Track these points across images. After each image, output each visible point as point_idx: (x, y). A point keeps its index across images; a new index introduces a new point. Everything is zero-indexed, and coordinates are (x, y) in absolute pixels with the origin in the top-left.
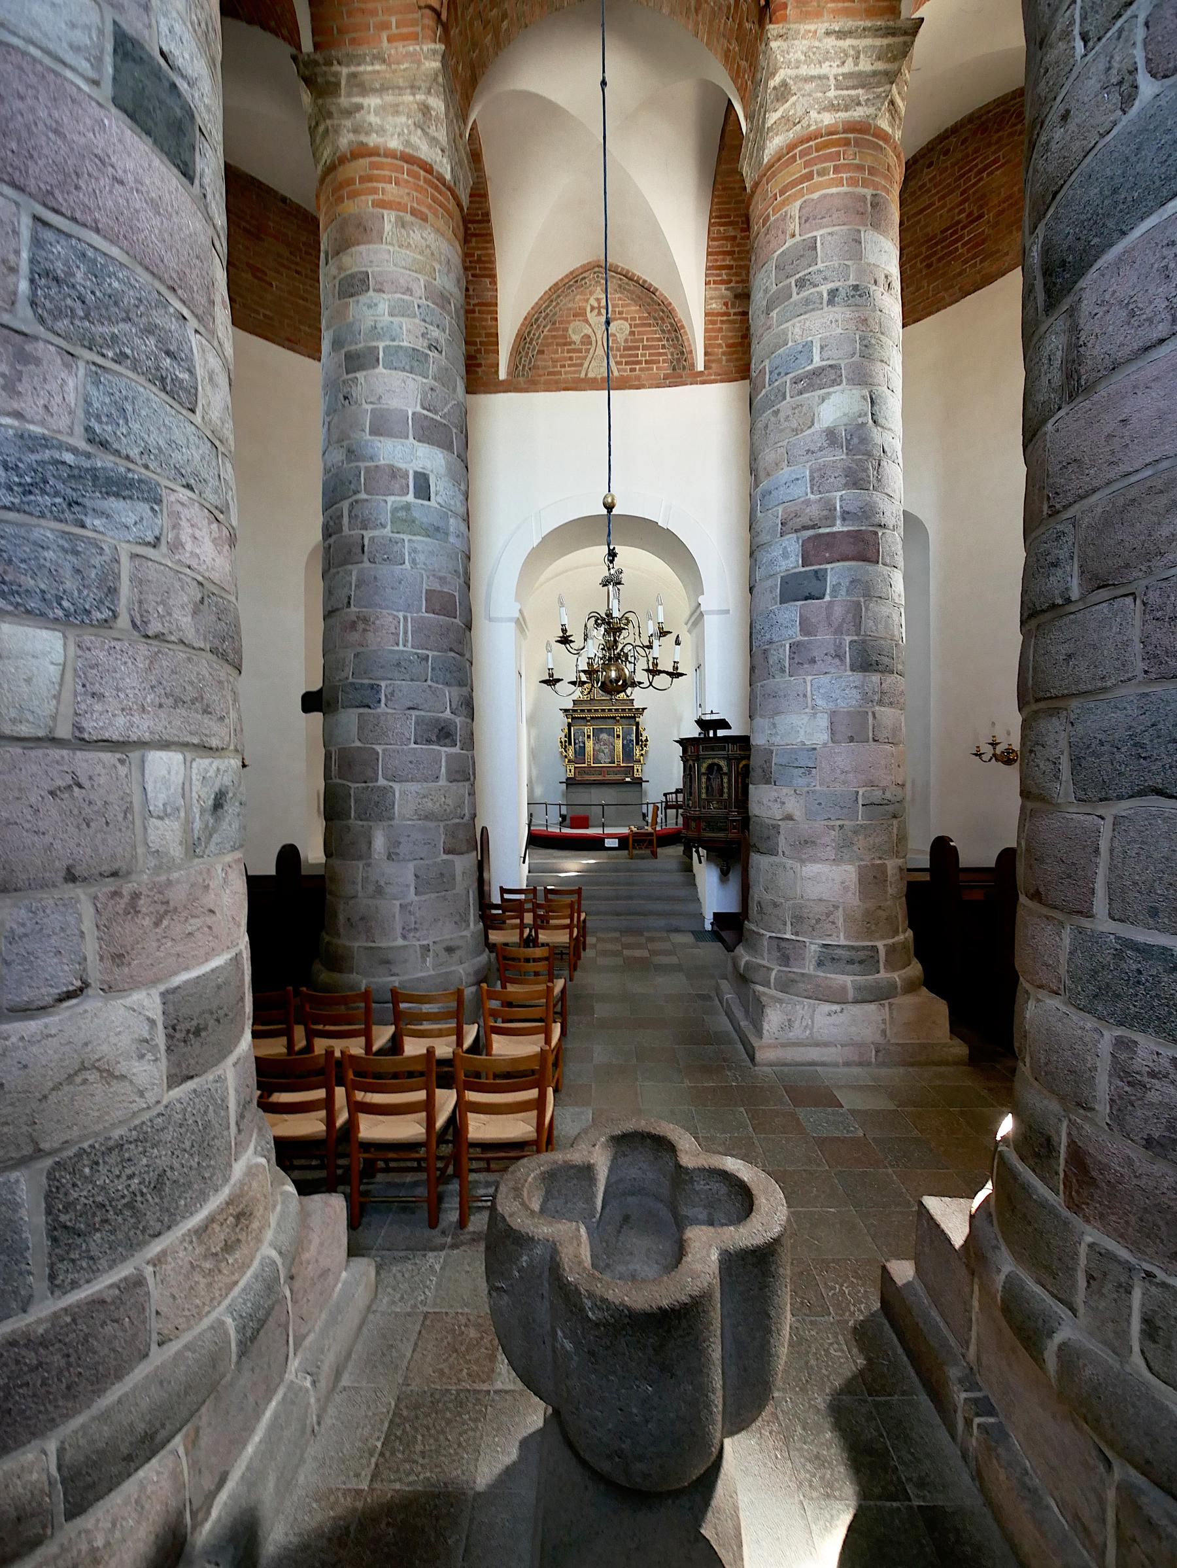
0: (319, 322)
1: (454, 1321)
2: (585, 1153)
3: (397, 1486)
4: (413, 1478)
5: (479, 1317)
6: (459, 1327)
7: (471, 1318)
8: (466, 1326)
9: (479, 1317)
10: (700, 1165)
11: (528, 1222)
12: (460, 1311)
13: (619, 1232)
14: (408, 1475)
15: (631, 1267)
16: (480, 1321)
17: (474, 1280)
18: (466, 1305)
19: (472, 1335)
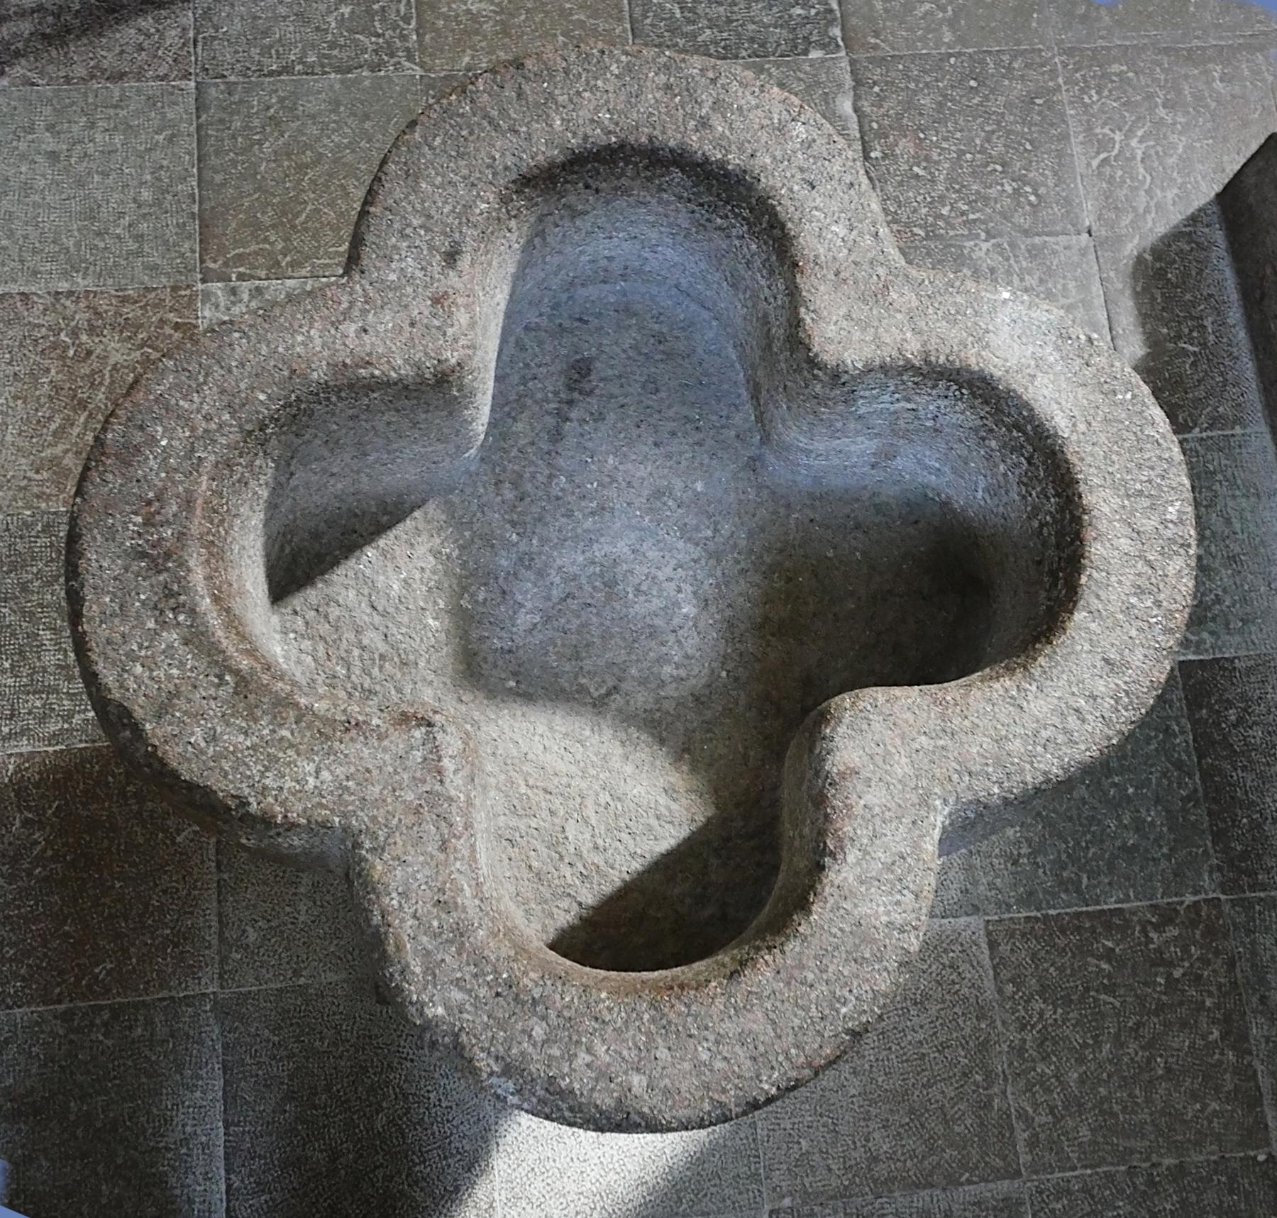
0: (1261, 372)
1: (50, 318)
2: (421, 308)
3: (25, 747)
4: (53, 727)
5: (124, 300)
6: (74, 334)
7: (103, 305)
8: (92, 330)
9: (124, 300)
10: (887, 354)
11: (234, 739)
12: (64, 286)
13: (557, 436)
14: (43, 719)
15: (598, 552)
16: (129, 311)
17: (81, 184)
18: (73, 266)
19: (115, 358)
